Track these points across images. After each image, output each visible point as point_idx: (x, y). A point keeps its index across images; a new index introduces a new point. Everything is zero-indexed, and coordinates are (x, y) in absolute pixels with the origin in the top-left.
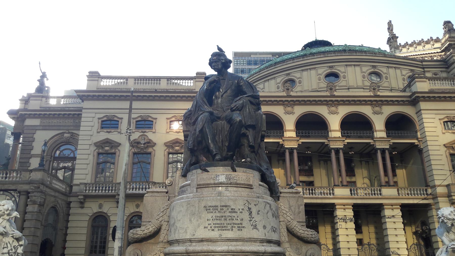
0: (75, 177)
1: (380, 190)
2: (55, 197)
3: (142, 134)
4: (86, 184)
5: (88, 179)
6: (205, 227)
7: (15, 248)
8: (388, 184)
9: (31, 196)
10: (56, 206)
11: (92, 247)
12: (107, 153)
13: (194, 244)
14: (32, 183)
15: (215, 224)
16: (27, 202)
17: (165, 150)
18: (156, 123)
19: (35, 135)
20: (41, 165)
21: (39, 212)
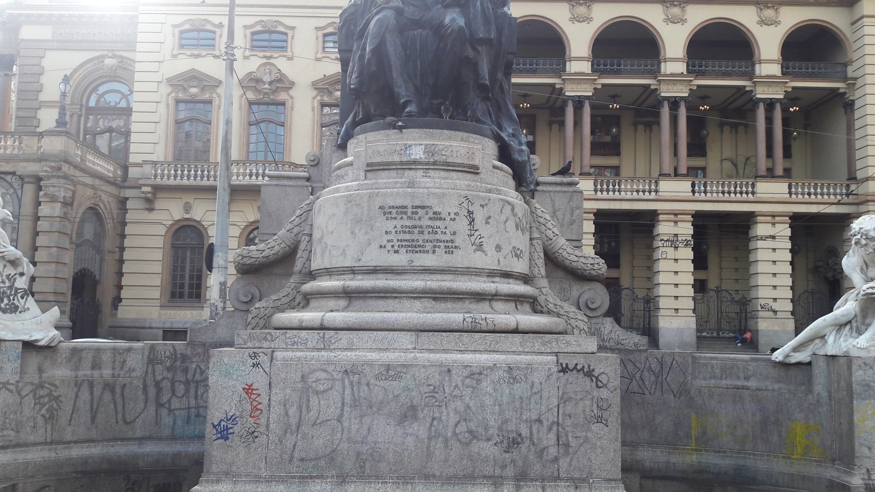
0: (133, 148)
1: (753, 186)
2: (93, 187)
3: (265, 61)
4: (155, 163)
5: (160, 153)
6: (381, 247)
7: (9, 280)
8: (770, 174)
9: (46, 187)
10: (98, 205)
11: (174, 285)
12: (193, 101)
13: (360, 277)
14: (46, 160)
15: (401, 240)
16: (38, 196)
17: (314, 98)
18: (293, 37)
19: (44, 60)
20: (61, 122)
21: (65, 217)
